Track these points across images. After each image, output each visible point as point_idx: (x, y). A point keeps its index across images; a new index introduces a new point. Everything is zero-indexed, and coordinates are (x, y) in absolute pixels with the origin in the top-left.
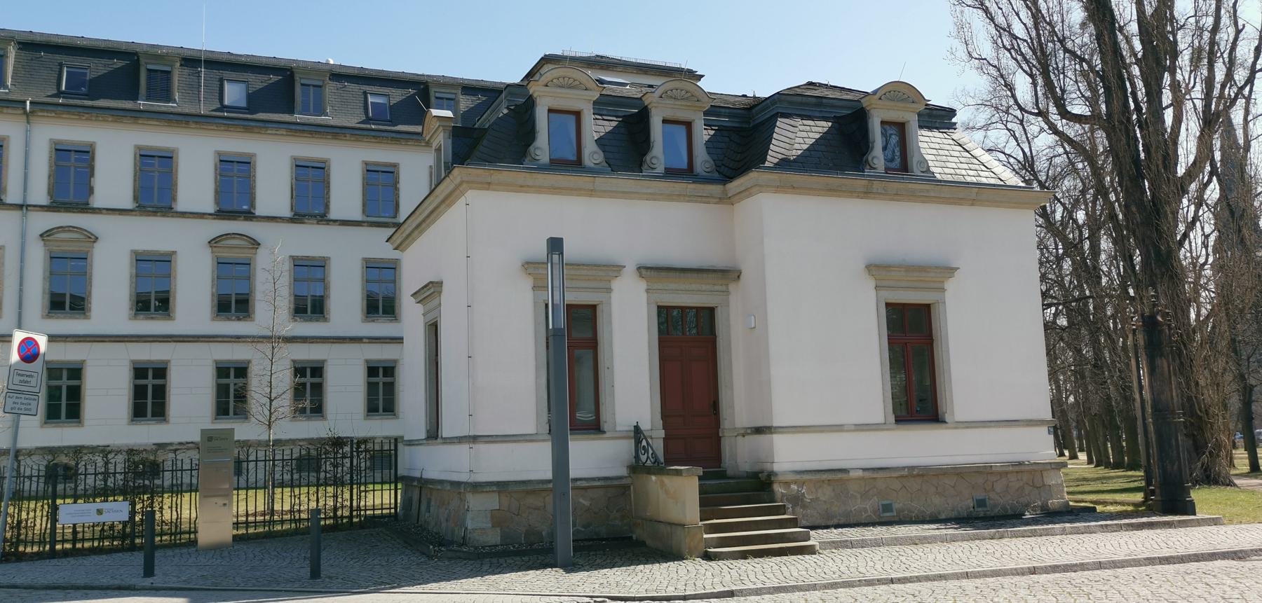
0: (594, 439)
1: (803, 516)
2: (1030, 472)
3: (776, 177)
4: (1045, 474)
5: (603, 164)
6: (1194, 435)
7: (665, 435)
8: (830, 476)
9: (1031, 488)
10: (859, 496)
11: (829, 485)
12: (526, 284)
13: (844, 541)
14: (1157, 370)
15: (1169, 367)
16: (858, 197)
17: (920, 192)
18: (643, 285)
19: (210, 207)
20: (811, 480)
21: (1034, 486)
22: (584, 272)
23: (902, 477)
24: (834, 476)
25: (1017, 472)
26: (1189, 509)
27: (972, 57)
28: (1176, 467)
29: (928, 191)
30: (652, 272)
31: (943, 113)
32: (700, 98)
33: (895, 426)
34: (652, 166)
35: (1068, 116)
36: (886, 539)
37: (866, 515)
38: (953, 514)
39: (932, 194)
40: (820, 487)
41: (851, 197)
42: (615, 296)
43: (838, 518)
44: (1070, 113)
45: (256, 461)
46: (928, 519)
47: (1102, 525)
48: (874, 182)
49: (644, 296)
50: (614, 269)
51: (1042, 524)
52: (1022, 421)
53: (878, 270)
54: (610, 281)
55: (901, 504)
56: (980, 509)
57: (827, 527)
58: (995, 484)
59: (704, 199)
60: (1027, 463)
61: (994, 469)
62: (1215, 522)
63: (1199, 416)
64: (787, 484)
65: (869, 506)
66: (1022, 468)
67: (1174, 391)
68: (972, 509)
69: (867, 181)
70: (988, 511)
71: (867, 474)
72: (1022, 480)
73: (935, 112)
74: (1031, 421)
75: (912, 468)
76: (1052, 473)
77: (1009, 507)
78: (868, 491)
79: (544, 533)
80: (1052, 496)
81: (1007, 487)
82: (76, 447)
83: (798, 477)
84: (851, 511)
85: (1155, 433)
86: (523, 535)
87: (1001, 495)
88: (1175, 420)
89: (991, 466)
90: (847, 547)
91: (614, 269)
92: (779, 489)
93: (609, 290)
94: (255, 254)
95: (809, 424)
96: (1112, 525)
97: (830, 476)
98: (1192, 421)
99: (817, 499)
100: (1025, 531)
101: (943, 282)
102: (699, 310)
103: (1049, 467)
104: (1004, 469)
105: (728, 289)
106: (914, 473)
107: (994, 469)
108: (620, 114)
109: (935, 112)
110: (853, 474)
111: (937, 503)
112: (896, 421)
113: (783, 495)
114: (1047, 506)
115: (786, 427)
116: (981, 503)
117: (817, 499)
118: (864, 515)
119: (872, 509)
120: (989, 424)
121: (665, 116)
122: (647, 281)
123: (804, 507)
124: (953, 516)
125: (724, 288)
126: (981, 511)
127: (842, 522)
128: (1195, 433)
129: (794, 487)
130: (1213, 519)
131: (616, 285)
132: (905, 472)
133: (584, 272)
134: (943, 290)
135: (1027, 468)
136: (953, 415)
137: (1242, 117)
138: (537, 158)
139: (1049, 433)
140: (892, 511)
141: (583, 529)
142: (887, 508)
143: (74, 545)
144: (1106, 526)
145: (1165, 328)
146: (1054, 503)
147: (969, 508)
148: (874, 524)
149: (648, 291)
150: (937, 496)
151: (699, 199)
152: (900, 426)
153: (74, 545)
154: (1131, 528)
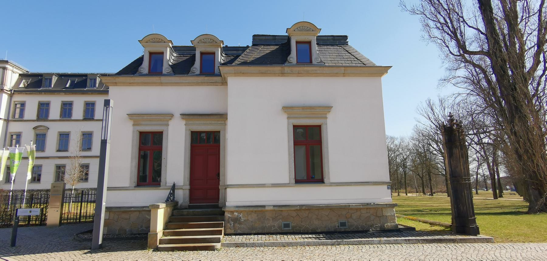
0: (155, 189)
1: (239, 228)
2: (375, 208)
3: (232, 69)
4: (384, 210)
5: (171, 72)
6: (539, 189)
7: (190, 188)
8: (256, 209)
9: (375, 217)
10: (271, 219)
11: (255, 213)
12: (131, 123)
13: (242, 243)
14: (454, 155)
15: (459, 153)
16: (279, 76)
17: (311, 71)
18: (184, 122)
19: (35, 118)
20: (245, 211)
21: (376, 216)
22: (154, 118)
23: (297, 210)
24: (258, 210)
25: (367, 209)
26: (476, 232)
27: (431, 37)
28: (465, 208)
29: (316, 70)
30: (187, 116)
31: (341, 38)
32: (217, 42)
33: (295, 185)
34: (194, 72)
35: (467, 52)
36: (267, 243)
37: (274, 228)
38: (325, 230)
39: (319, 72)
40: (250, 214)
41: (275, 76)
42: (170, 128)
43: (258, 229)
44: (468, 51)
45: (91, 195)
46: (310, 232)
47: (406, 240)
48: (285, 68)
49: (286, 121)
50: (171, 116)
51: (365, 238)
52: (371, 182)
53: (288, 109)
54: (168, 121)
55: (295, 224)
56: (341, 227)
57: (250, 234)
58: (352, 214)
59: (214, 84)
60: (372, 204)
61: (351, 207)
62: (487, 241)
63: (540, 180)
64: (232, 212)
65: (277, 224)
66: (369, 206)
67: (462, 166)
68: (337, 227)
69: (281, 68)
70: (347, 228)
71: (276, 209)
72: (369, 213)
73: (336, 38)
74: (376, 182)
75: (302, 206)
76: (389, 209)
77: (360, 227)
78: (277, 216)
79: (127, 230)
80: (387, 221)
81: (360, 216)
82: (23, 190)
83: (237, 209)
84: (266, 226)
85: (452, 189)
86: (117, 231)
87: (356, 220)
88: (463, 182)
89: (349, 205)
90: (244, 247)
91: (171, 116)
92: (227, 215)
93: (168, 125)
94: (48, 131)
95: (246, 184)
96: (413, 239)
97: (256, 209)
98: (537, 182)
99: (248, 220)
100: (355, 241)
101: (326, 114)
102: (208, 133)
103: (385, 206)
104: (359, 207)
105: (225, 123)
106: (303, 208)
107: (351, 207)
108: (192, 54)
109: (336, 38)
110: (267, 208)
111: (316, 224)
112: (295, 182)
113: (229, 217)
114: (384, 226)
115: (234, 185)
116: (343, 224)
117: (248, 220)
118: (273, 229)
119: (278, 226)
120: (350, 184)
121: (201, 51)
122: (186, 121)
123: (240, 223)
124: (325, 231)
125: (223, 122)
126: (343, 229)
127: (260, 232)
128: (539, 188)
129: (236, 214)
130: (486, 239)
131: (171, 123)
132: (298, 208)
133: (154, 118)
134: (326, 118)
135: (371, 207)
136: (329, 180)
137: (526, 29)
138: (141, 72)
139: (388, 189)
140: (289, 227)
141: (145, 229)
142: (287, 225)
143: (67, 221)
144: (409, 240)
145: (457, 132)
146: (389, 225)
147: (336, 227)
148: (276, 234)
149: (185, 125)
150: (317, 220)
151: (212, 84)
152: (297, 185)
153: (67, 221)
154: (426, 242)
